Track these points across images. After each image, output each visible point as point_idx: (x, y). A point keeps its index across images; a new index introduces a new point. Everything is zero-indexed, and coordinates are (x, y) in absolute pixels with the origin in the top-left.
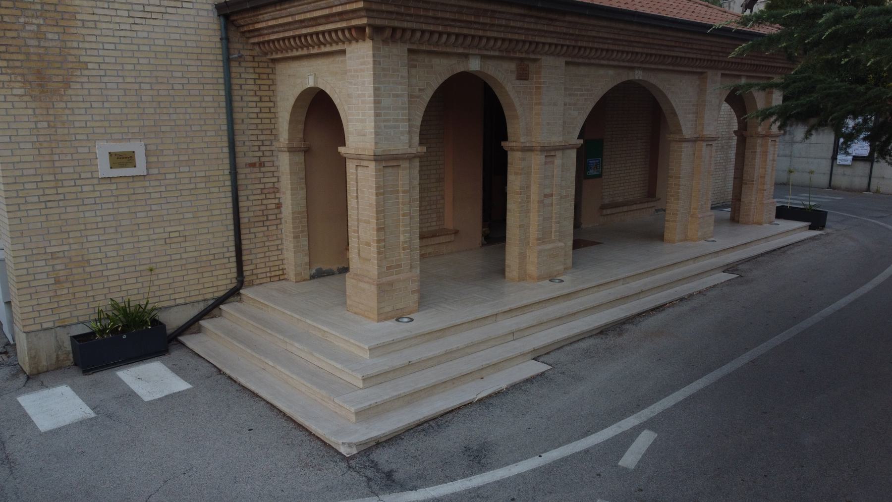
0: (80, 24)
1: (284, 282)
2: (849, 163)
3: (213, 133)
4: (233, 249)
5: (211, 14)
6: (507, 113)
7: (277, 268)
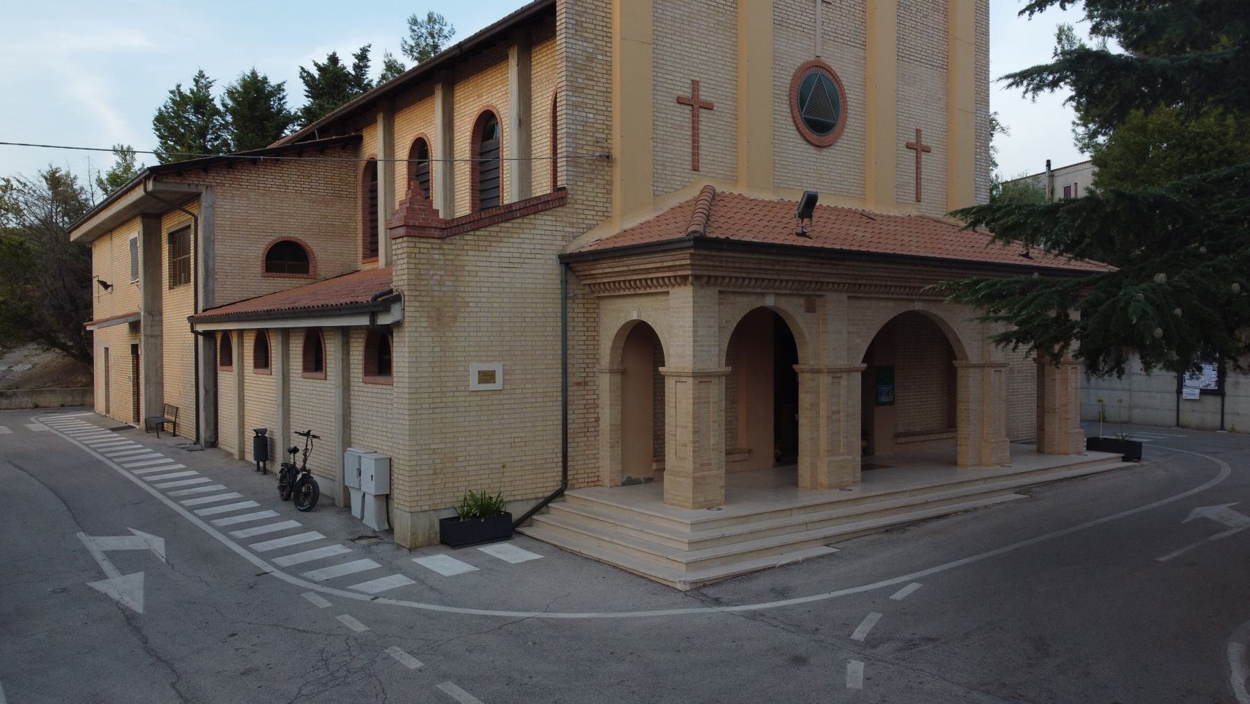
0: (467, 273)
1: (599, 488)
2: (1197, 397)
3: (551, 357)
4: (560, 455)
5: (555, 262)
6: (797, 340)
7: (593, 475)
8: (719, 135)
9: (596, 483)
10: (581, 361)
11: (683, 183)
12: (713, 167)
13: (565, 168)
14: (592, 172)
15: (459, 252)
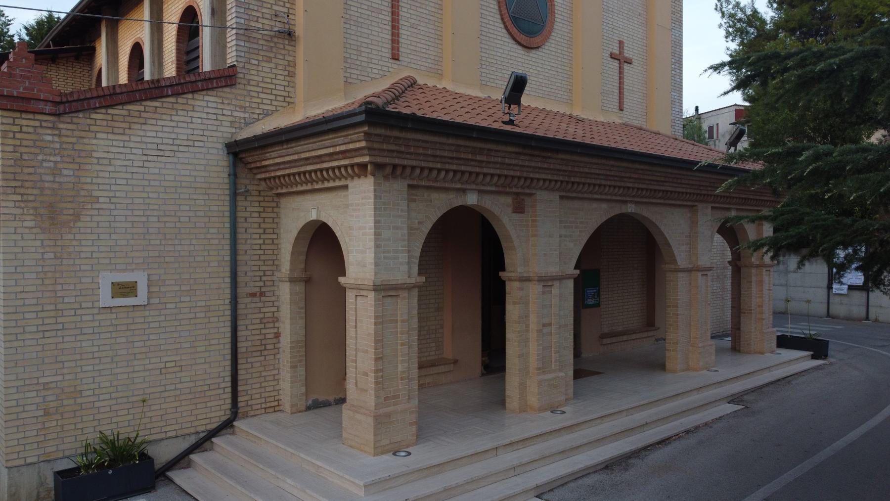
2: (845, 292)
4: (229, 379)
6: (504, 245)
7: (272, 399)
8: (422, 24)
9: (276, 408)
10: (256, 268)
11: (382, 73)
12: (415, 57)
13: (234, 43)
14: (270, 49)
15: (83, 134)
